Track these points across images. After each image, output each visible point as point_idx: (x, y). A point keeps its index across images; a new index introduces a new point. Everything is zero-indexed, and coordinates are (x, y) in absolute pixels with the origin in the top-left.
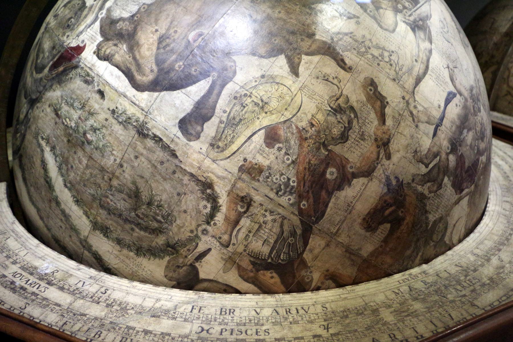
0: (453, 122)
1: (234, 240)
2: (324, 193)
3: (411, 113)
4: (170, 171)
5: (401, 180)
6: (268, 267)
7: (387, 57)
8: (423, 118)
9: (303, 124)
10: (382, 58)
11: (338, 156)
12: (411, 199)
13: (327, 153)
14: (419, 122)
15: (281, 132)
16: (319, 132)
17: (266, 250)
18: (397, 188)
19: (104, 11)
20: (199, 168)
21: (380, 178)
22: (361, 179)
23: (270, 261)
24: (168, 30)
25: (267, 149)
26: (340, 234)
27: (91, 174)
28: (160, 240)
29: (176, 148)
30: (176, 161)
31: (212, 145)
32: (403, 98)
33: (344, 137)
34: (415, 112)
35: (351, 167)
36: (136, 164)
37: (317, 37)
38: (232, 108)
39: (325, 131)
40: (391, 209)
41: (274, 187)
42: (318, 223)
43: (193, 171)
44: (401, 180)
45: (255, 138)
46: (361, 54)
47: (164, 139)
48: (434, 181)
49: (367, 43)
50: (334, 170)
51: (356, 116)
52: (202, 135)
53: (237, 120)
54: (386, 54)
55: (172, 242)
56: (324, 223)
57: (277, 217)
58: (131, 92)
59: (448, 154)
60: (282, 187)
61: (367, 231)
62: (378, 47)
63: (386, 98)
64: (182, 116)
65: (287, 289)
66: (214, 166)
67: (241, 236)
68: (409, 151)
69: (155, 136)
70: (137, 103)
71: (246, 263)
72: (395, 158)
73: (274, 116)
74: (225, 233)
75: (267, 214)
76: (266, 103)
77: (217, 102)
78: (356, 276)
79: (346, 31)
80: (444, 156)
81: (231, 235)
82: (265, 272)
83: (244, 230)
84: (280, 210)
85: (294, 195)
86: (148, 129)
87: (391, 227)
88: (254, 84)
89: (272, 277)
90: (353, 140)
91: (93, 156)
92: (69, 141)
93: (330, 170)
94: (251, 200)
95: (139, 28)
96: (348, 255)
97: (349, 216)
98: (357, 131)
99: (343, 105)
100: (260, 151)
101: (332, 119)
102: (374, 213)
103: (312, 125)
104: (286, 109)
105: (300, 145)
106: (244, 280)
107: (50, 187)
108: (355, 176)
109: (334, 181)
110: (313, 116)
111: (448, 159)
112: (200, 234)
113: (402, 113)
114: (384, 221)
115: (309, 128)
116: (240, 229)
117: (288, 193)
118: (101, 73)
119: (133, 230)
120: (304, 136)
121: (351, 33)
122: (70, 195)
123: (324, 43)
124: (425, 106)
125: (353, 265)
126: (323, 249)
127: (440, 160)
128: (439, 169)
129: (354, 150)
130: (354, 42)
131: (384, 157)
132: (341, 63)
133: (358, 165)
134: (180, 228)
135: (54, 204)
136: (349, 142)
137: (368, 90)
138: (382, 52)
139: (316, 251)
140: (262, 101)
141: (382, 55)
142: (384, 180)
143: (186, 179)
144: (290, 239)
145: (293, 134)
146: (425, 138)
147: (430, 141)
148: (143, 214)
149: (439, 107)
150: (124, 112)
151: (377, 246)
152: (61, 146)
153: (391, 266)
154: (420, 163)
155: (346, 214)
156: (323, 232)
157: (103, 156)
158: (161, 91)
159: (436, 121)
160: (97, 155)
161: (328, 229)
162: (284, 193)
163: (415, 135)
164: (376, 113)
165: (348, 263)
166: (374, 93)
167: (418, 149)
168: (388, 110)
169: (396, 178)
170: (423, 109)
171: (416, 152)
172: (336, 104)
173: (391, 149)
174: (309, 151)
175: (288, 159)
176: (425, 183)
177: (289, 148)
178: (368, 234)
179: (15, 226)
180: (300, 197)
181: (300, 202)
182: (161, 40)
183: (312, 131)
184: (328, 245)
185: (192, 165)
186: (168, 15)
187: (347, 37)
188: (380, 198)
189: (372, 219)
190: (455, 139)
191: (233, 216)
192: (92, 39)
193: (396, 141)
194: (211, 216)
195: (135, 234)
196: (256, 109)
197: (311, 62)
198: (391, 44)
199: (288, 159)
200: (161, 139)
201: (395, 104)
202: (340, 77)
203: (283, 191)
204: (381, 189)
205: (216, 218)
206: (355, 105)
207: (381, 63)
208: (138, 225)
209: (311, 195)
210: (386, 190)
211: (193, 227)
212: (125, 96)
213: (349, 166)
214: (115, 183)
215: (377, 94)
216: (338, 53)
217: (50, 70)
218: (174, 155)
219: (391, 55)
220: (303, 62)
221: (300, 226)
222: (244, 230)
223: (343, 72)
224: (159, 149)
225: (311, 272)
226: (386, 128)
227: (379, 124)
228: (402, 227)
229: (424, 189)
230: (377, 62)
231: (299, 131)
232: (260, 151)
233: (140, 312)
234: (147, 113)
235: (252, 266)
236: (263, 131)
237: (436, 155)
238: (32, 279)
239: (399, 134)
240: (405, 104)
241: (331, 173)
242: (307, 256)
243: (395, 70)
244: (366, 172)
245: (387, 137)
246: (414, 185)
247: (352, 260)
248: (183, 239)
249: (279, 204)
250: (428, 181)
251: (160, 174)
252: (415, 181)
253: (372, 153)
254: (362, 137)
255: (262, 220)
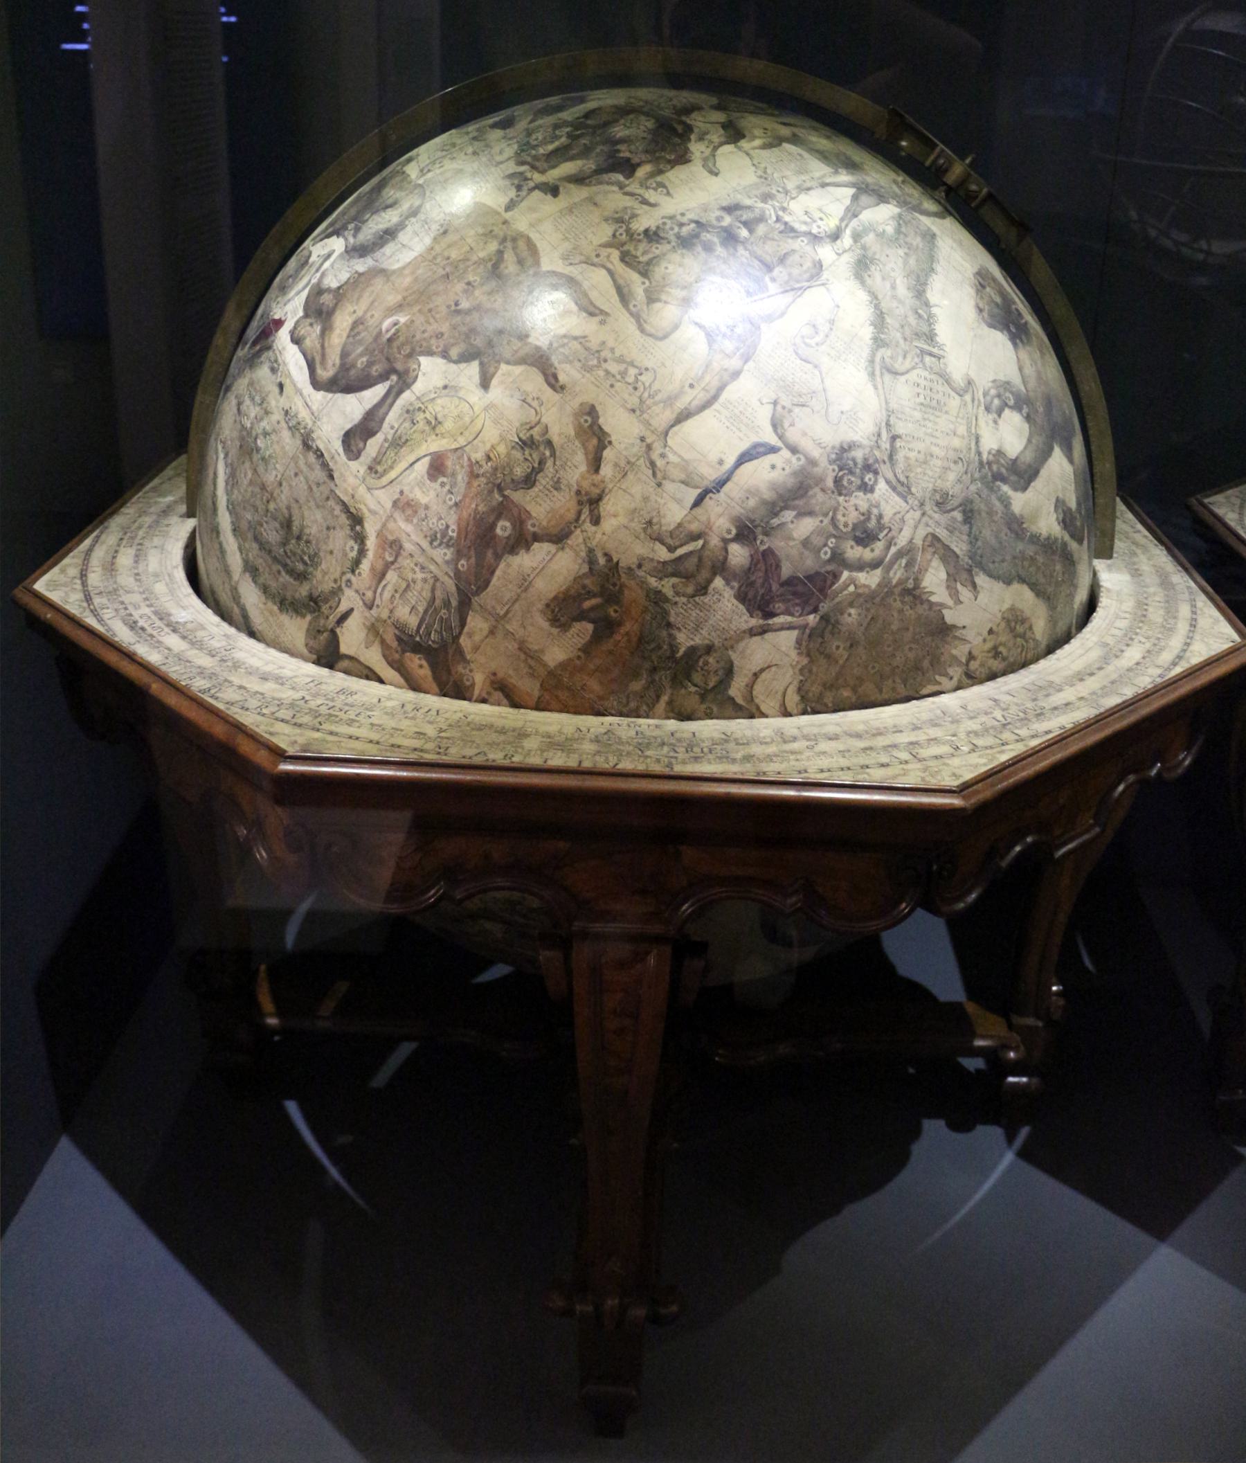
0: (750, 493)
1: (378, 601)
2: (490, 554)
3: (653, 464)
4: (324, 496)
5: (615, 560)
6: (417, 648)
7: (633, 377)
8: (677, 474)
9: (478, 456)
10: (623, 378)
11: (517, 506)
12: (633, 593)
13: (501, 499)
14: (664, 478)
15: (449, 463)
16: (495, 469)
17: (413, 621)
18: (606, 570)
19: (318, 275)
20: (353, 497)
21: (578, 549)
22: (547, 544)
23: (418, 639)
24: (365, 312)
25: (428, 482)
26: (510, 619)
27: (252, 492)
28: (303, 590)
29: (334, 468)
30: (332, 485)
31: (370, 468)
32: (642, 439)
33: (529, 481)
34: (660, 463)
35: (534, 526)
36: (294, 484)
37: (530, 340)
38: (401, 424)
39: (504, 469)
40: (594, 602)
41: (428, 534)
42: (478, 595)
43: (345, 499)
44: (615, 560)
45: (418, 466)
46: (588, 369)
47: (326, 455)
48: (687, 578)
49: (606, 354)
50: (508, 524)
51: (553, 454)
52: (363, 454)
53: (403, 440)
54: (632, 372)
55: (316, 594)
56: (486, 598)
57: (429, 576)
58: (308, 389)
59: (726, 542)
60: (439, 536)
61: (552, 625)
62: (621, 360)
63: (609, 436)
64: (348, 426)
65: (441, 690)
66: (368, 496)
67: (387, 595)
68: (636, 520)
69: (318, 449)
70: (310, 404)
71: (390, 637)
72: (608, 524)
73: (444, 441)
74: (369, 588)
75: (417, 569)
76: (440, 423)
77: (387, 414)
78: (539, 698)
79: (577, 333)
80: (714, 541)
81: (375, 592)
82: (413, 655)
83: (389, 588)
84: (432, 567)
85: (452, 549)
86: (313, 440)
87: (595, 630)
88: (433, 396)
89: (421, 666)
90: (541, 487)
91: (258, 469)
92: (241, 446)
93: (501, 523)
94: (401, 547)
95: (340, 304)
96: (523, 656)
97: (523, 595)
98: (550, 475)
99: (537, 437)
100: (420, 484)
101: (518, 454)
102: (564, 600)
103: (489, 458)
104: (461, 434)
105: (468, 483)
106: (388, 663)
107: (215, 509)
108: (536, 538)
109: (504, 541)
110: (492, 446)
111: (726, 551)
112: (343, 585)
113: (633, 460)
114: (582, 616)
115: (483, 463)
116: (385, 586)
117: (444, 545)
118: (287, 361)
119: (279, 572)
120: (476, 472)
121: (585, 337)
122: (229, 520)
123: (538, 348)
124: (686, 456)
125: (532, 675)
126: (487, 637)
127: (703, 546)
128: (700, 559)
129: (542, 502)
130: (583, 351)
131: (588, 520)
132: (552, 380)
133: (544, 523)
134: (325, 573)
135: (214, 535)
136: (536, 489)
137: (582, 420)
138: (626, 369)
139: (477, 638)
140: (436, 419)
141: (623, 374)
142: (583, 554)
143: (338, 509)
144: (443, 611)
145: (462, 467)
146: (673, 506)
147: (685, 512)
148: (291, 551)
149: (721, 462)
150: (296, 415)
151: (571, 655)
152: (233, 452)
153: (601, 698)
154: (657, 543)
155: (519, 591)
156: (486, 610)
157: (266, 470)
158: (335, 392)
159: (706, 483)
160: (261, 469)
161: (493, 607)
162: (440, 545)
163: (653, 497)
164: (586, 454)
165: (525, 671)
166: (591, 426)
167: (655, 520)
168: (607, 453)
169: (606, 554)
170: (679, 460)
171: (650, 523)
172: (528, 435)
173: (601, 509)
174: (478, 493)
175: (450, 499)
176: (666, 576)
177: (453, 485)
178: (555, 631)
179: (175, 571)
180: (459, 554)
181: (458, 560)
182: (355, 324)
183: (487, 467)
184: (492, 632)
185: (346, 491)
186: (373, 292)
187: (575, 342)
188: (575, 579)
189: (560, 609)
190: (752, 521)
191: (379, 566)
192: (295, 312)
193: (612, 499)
194: (357, 563)
195: (281, 579)
196: (427, 428)
197: (509, 374)
198: (650, 356)
199: (450, 499)
200: (322, 455)
201: (623, 446)
202: (544, 399)
203: (438, 542)
204: (577, 567)
205: (361, 566)
206: (556, 440)
207: (618, 385)
208: (285, 566)
209: (472, 553)
210: (585, 568)
211: (337, 575)
212: (301, 394)
213: (530, 522)
214: (272, 506)
215: (596, 428)
216: (552, 365)
217: (250, 348)
218: (331, 477)
219: (641, 374)
220: (500, 372)
221: (456, 594)
222: (389, 588)
223: (549, 391)
224: (318, 467)
225: (471, 671)
226: (599, 477)
227: (588, 472)
228: (617, 637)
229: (667, 586)
230: (609, 383)
231: (471, 465)
232: (420, 484)
233: (251, 672)
234: (315, 417)
235: (396, 643)
236: (427, 459)
237: (694, 537)
238: (158, 623)
239: (620, 491)
240: (644, 449)
241: (503, 528)
242: (464, 641)
243: (640, 398)
244: (556, 535)
245: (598, 491)
246: (641, 573)
247: (530, 667)
248: (327, 591)
249: (432, 559)
250: (673, 575)
251: (315, 499)
252: (644, 568)
253: (569, 510)
254: (557, 486)
255: (410, 576)
